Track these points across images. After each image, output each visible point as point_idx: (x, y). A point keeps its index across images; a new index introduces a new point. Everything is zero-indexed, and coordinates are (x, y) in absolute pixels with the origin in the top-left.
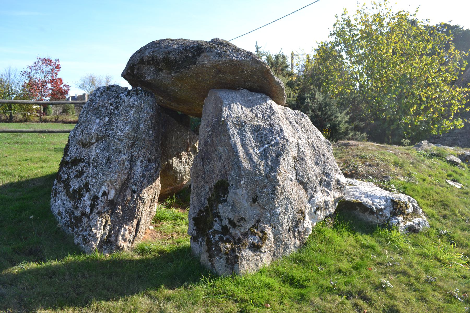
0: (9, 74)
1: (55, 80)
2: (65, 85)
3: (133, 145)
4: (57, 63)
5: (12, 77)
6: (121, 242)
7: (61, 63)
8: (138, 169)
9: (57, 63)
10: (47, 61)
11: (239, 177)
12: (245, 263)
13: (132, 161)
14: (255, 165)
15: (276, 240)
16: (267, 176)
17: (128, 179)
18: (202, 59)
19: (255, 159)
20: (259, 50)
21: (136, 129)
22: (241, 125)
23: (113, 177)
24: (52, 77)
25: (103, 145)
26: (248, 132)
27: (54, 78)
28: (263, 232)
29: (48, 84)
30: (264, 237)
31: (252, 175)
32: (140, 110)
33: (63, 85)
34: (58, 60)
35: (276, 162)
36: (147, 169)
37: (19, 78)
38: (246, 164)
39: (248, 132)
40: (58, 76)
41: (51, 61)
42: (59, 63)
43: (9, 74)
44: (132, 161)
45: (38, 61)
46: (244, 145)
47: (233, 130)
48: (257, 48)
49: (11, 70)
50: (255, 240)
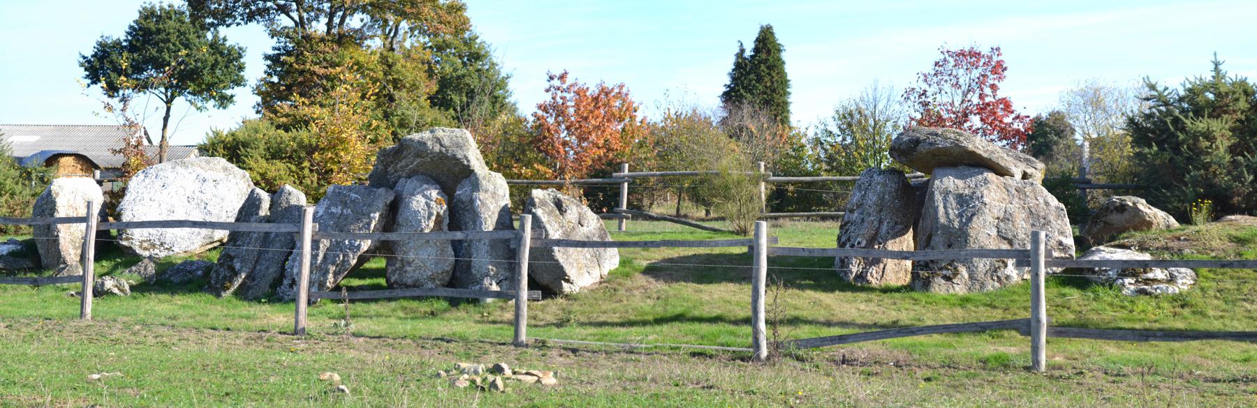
0: (875, 99)
1: (988, 104)
2: (1018, 117)
3: (881, 210)
4: (995, 59)
5: (880, 107)
6: (869, 277)
7: (1006, 58)
8: (884, 227)
9: (995, 59)
10: (969, 57)
11: (937, 228)
12: (936, 287)
13: (880, 222)
14: (950, 221)
15: (971, 277)
16: (960, 229)
17: (876, 234)
18: (920, 147)
19: (952, 217)
20: (1220, 67)
21: (882, 199)
22: (946, 193)
23: (864, 231)
24: (981, 97)
25: (860, 210)
26: (951, 198)
27: (987, 100)
28: (956, 268)
29: (972, 117)
30: (956, 273)
31: (947, 229)
32: (885, 185)
33: (1013, 116)
34: (998, 49)
35: (970, 219)
36: (892, 228)
37: (897, 107)
38: (942, 220)
39: (951, 198)
40: (1000, 94)
41: (978, 55)
42: (1000, 58)
43: (875, 99)
44: (880, 222)
45: (945, 60)
46: (945, 207)
47: (938, 198)
48: (1217, 65)
49: (879, 89)
50: (949, 273)
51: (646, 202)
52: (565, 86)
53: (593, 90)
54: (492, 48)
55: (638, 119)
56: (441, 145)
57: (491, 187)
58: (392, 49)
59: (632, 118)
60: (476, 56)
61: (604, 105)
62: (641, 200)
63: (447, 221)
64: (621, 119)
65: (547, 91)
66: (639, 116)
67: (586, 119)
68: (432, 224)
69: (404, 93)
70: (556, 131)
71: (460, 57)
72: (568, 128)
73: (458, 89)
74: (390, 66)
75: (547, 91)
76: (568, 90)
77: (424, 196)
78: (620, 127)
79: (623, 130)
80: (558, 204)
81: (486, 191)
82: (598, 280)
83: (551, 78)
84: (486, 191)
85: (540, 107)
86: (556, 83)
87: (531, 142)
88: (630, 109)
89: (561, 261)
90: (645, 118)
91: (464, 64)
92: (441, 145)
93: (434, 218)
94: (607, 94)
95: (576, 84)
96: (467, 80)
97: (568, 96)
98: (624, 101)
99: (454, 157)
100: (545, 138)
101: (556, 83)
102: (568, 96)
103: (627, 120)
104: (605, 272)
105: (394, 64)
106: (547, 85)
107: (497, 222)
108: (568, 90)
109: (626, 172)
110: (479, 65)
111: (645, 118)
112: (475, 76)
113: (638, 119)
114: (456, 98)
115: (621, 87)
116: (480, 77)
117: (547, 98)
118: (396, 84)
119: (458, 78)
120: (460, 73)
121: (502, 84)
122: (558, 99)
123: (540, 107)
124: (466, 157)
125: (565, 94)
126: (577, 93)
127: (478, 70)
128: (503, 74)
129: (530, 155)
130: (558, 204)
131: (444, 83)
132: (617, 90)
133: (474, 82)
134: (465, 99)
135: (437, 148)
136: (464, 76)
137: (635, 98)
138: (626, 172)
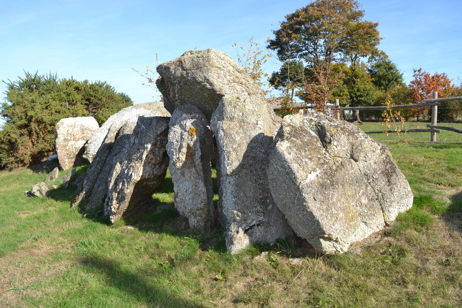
51: (454, 116)
52: (420, 74)
53: (432, 74)
54: (396, 65)
55: (451, 85)
56: (183, 69)
57: (237, 114)
58: (355, 65)
59: (448, 85)
60: (391, 68)
61: (438, 81)
62: (453, 115)
63: (198, 154)
64: (444, 86)
65: (414, 76)
66: (451, 84)
67: (429, 85)
68: (183, 157)
69: (358, 80)
70: (418, 91)
71: (385, 69)
72: (422, 89)
73: (385, 80)
74: (354, 71)
75: (414, 76)
76: (422, 75)
77: (181, 126)
78: (444, 89)
79: (445, 89)
80: (321, 132)
81: (232, 119)
82: (381, 227)
83: (415, 71)
84: (232, 119)
85: (411, 82)
86: (417, 73)
87: (408, 95)
88: (448, 82)
89: (317, 214)
90: (454, 85)
91: (387, 71)
92: (183, 69)
93: (184, 150)
94: (438, 77)
95: (425, 73)
96: (388, 76)
97: (422, 77)
98: (445, 79)
99: (195, 82)
100: (413, 93)
101: (417, 73)
102: (422, 77)
103: (446, 86)
104: (392, 217)
105: (355, 70)
106: (414, 74)
107: (246, 156)
108: (422, 75)
109: (436, 98)
110: (392, 71)
111: (454, 85)
112: (390, 75)
113: (451, 85)
114: (384, 83)
115: (444, 74)
116: (392, 75)
117: (414, 79)
118: (356, 76)
119: (385, 76)
120: (385, 74)
121: (401, 77)
122: (418, 79)
123: (411, 82)
124: (208, 81)
125: (421, 77)
126: (425, 76)
127: (392, 73)
128: (400, 74)
129: (408, 100)
130: (321, 132)
131: (380, 77)
132: (442, 76)
133: (390, 77)
134: (387, 83)
135: (179, 72)
136: (386, 75)
137: (450, 77)
138: (436, 98)
